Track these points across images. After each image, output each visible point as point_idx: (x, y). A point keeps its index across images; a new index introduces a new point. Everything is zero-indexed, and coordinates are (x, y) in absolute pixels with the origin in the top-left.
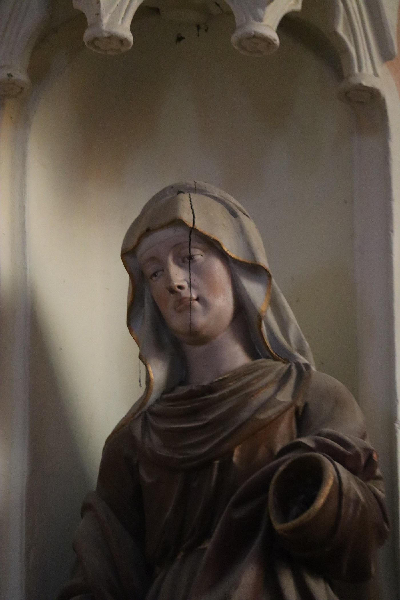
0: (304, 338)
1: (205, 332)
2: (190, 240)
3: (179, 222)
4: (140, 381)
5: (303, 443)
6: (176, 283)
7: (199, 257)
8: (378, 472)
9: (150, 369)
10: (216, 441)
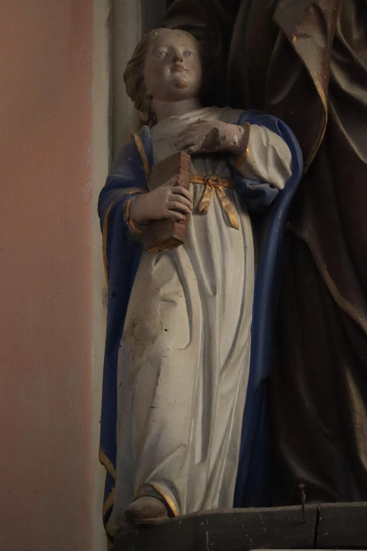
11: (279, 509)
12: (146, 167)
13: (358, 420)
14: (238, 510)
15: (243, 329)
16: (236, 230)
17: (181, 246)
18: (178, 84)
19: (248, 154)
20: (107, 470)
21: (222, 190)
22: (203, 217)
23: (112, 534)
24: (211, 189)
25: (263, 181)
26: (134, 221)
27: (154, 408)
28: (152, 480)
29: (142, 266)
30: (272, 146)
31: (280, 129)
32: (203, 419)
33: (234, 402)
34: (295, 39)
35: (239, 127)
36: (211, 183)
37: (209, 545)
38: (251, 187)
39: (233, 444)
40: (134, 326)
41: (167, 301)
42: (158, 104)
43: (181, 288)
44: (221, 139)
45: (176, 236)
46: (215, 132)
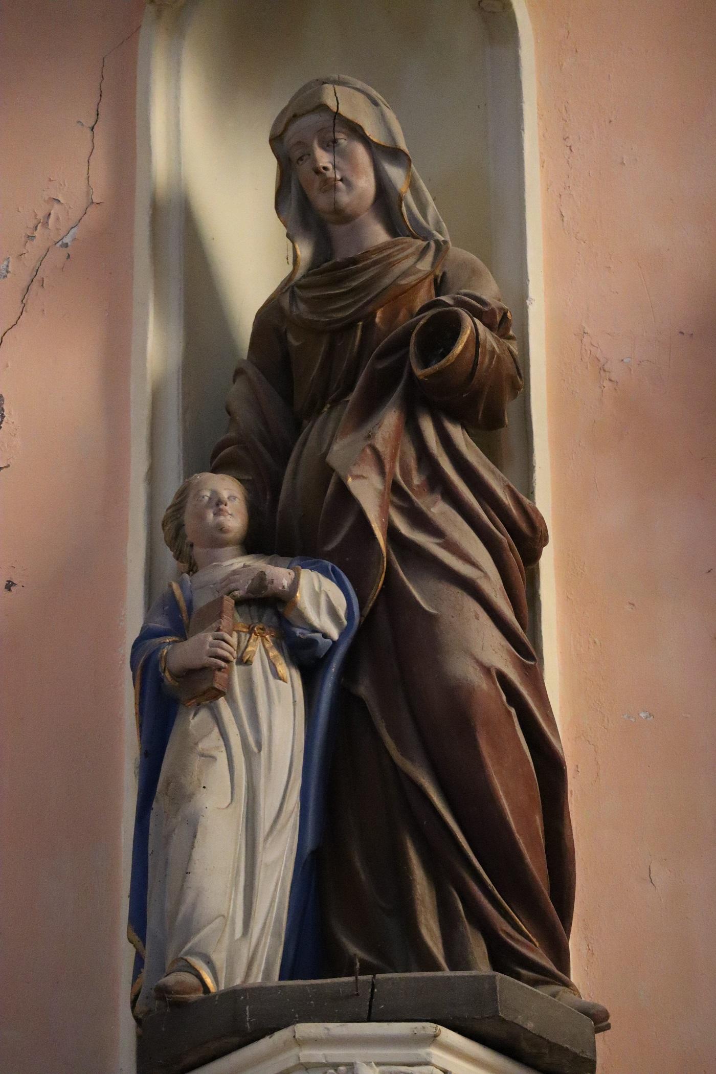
0: (442, 220)
1: (348, 211)
2: (334, 125)
3: (324, 108)
4: (287, 259)
5: (442, 300)
6: (321, 164)
7: (342, 141)
8: (511, 333)
9: (297, 246)
10: (360, 304)
11: (329, 981)
12: (185, 616)
13: (419, 891)
14: (283, 983)
15: (289, 796)
16: (284, 683)
17: (223, 698)
18: (221, 529)
19: (299, 598)
20: (136, 948)
21: (270, 641)
22: (247, 667)
23: (140, 1016)
24: (257, 638)
25: (315, 630)
26: (170, 672)
27: (190, 873)
28: (187, 953)
29: (178, 722)
30: (325, 591)
31: (334, 575)
32: (245, 890)
33: (280, 872)
34: (350, 480)
35: (289, 570)
36: (257, 632)
37: (249, 1021)
38: (301, 636)
39: (278, 920)
40: (168, 784)
41: (205, 756)
42: (199, 552)
43: (222, 743)
44: (269, 583)
45: (216, 686)
46: (262, 576)
